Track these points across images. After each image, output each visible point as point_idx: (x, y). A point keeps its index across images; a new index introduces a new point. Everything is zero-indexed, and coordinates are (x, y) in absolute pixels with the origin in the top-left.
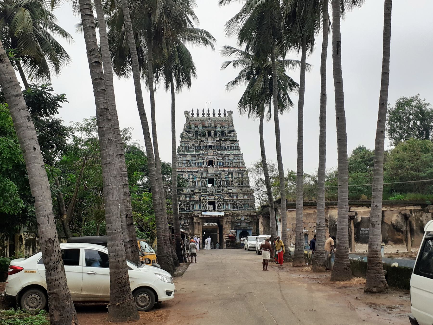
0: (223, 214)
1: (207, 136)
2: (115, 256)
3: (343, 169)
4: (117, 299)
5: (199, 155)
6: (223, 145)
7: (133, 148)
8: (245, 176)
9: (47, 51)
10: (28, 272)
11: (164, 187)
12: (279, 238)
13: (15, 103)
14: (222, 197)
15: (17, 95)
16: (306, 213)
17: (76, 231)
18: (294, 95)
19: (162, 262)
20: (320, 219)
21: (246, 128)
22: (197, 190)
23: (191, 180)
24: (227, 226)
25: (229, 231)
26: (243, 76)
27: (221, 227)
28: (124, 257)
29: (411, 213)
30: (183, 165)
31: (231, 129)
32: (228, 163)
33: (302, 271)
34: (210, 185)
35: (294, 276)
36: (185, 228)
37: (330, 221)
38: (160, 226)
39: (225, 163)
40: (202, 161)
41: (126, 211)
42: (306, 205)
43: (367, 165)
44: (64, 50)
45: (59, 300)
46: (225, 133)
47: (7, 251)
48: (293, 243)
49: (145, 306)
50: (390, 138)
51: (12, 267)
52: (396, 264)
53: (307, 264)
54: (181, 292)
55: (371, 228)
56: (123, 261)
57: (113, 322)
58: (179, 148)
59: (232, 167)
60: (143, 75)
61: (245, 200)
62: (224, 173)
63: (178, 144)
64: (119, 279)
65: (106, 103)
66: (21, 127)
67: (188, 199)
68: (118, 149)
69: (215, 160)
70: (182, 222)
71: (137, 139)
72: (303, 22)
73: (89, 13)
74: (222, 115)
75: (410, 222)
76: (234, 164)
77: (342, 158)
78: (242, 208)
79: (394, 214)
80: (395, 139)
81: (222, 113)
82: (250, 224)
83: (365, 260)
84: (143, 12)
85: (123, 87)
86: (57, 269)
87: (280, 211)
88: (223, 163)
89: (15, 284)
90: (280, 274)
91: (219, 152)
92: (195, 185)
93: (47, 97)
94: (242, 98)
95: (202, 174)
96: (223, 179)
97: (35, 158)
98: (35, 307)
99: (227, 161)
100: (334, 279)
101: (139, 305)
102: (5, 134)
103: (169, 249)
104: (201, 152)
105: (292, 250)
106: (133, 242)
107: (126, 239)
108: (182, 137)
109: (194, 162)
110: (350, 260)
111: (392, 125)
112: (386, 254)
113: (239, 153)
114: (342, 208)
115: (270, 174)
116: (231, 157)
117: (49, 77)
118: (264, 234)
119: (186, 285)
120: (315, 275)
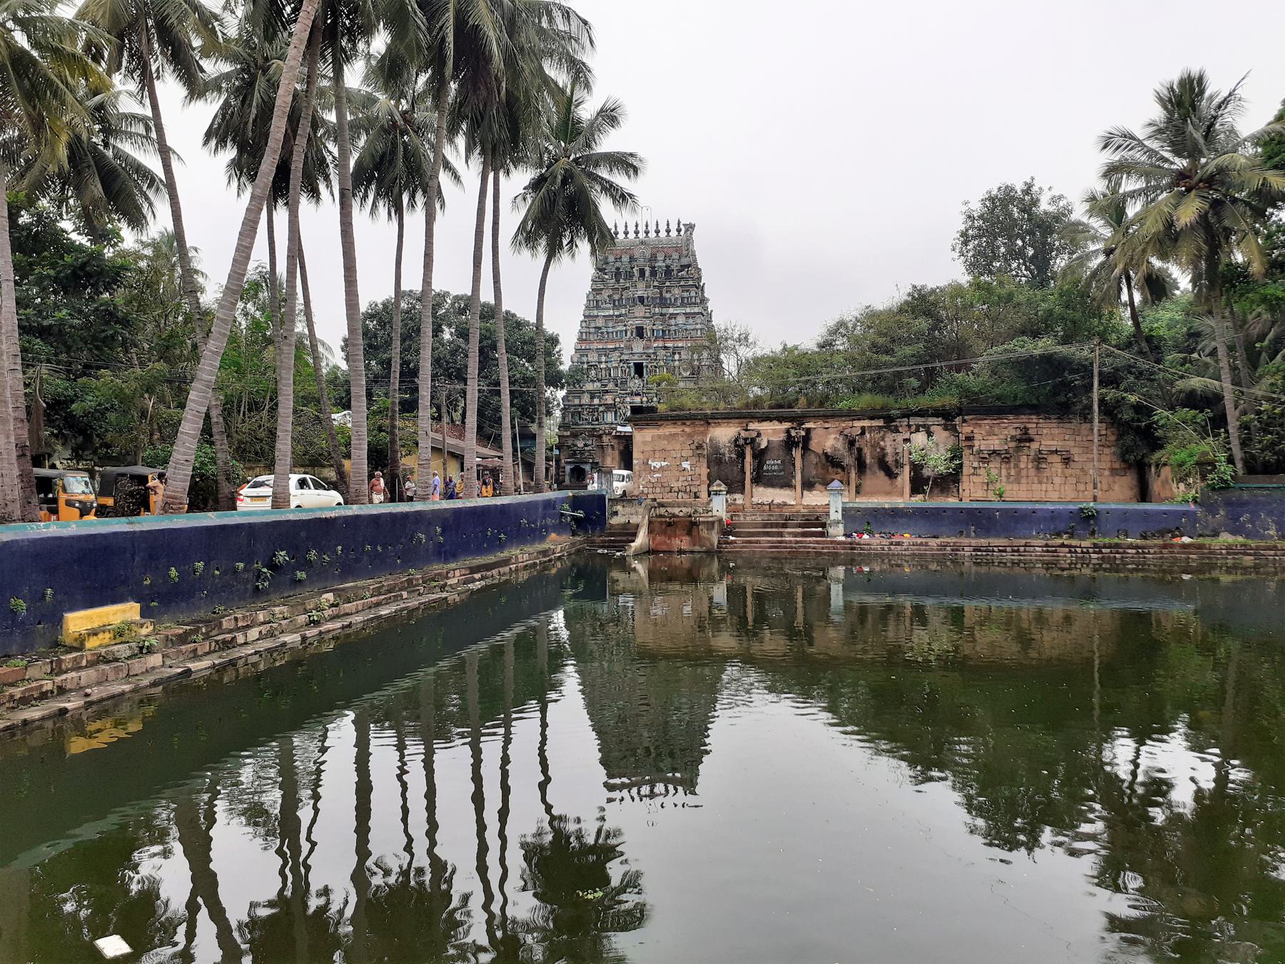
6: (668, 295)
29: (863, 433)
31: (685, 261)
62: (664, 352)
69: (648, 326)
74: (674, 234)
75: (860, 450)
81: (673, 227)
99: (673, 328)
116: (681, 320)
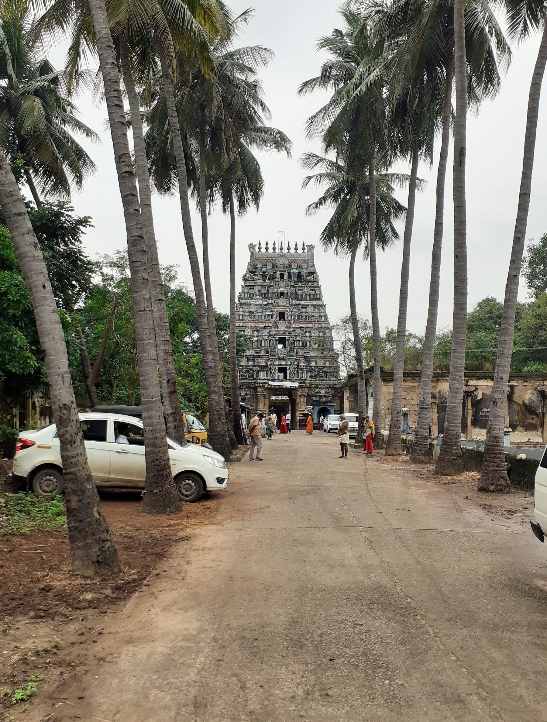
0: (296, 384)
1: (278, 279)
2: (152, 431)
3: (459, 327)
4: (154, 485)
5: (267, 304)
6: (300, 292)
7: (180, 293)
8: (328, 334)
9: (65, 158)
10: (42, 447)
11: (219, 347)
12: (368, 417)
13: (18, 225)
14: (296, 363)
15: (19, 214)
16: (407, 387)
17: (105, 399)
18: (399, 224)
19: (215, 442)
20: (425, 393)
21: (331, 267)
22: (263, 353)
23: (255, 339)
24: (302, 400)
25: (303, 407)
26: (329, 196)
27: (293, 402)
28: (164, 433)
30: (245, 318)
31: (311, 270)
32: (306, 316)
33: (396, 461)
34: (280, 346)
35: (386, 466)
36: (247, 400)
37: (440, 397)
38: (213, 396)
39: (302, 316)
40: (271, 313)
41: (168, 374)
42: (407, 375)
43: (495, 323)
44: (87, 156)
45: (77, 482)
46: (303, 275)
47: (17, 421)
48: (388, 425)
49: (190, 495)
50: (530, 287)
51: (20, 440)
52: (523, 456)
53: (405, 452)
54: (237, 480)
55: (492, 407)
56: (163, 438)
57: (148, 513)
58: (241, 295)
59: (310, 323)
60: (192, 194)
61: (327, 367)
63: (238, 289)
64: (157, 460)
65: (139, 228)
66: (26, 257)
67: (251, 363)
68: (157, 293)
70: (243, 394)
71: (183, 281)
72: (418, 120)
73: (118, 103)
74: (300, 251)
76: (314, 319)
77: (459, 311)
78: (322, 377)
79: (528, 390)
80: (536, 289)
81: (300, 247)
82: (332, 399)
83: (482, 449)
84: (193, 104)
85: (165, 208)
86: (74, 443)
87: (372, 383)
88: (298, 316)
89: (25, 462)
90: (368, 463)
91: (294, 301)
92: (261, 345)
93: (66, 220)
94: (327, 227)
95: (270, 331)
96: (298, 338)
97: (45, 298)
98: (51, 492)
99: (304, 315)
100: (438, 472)
101: (183, 494)
102: (10, 268)
103: (224, 427)
104: (270, 301)
105: (386, 434)
106: (177, 415)
107: (167, 410)
108: (245, 279)
109: (260, 314)
110: (462, 449)
111: (533, 269)
112: (512, 443)
113: (320, 303)
114: (454, 379)
115: (361, 334)
116: (310, 309)
117: (68, 192)
118: (350, 412)
119: (244, 472)
120: (413, 467)
